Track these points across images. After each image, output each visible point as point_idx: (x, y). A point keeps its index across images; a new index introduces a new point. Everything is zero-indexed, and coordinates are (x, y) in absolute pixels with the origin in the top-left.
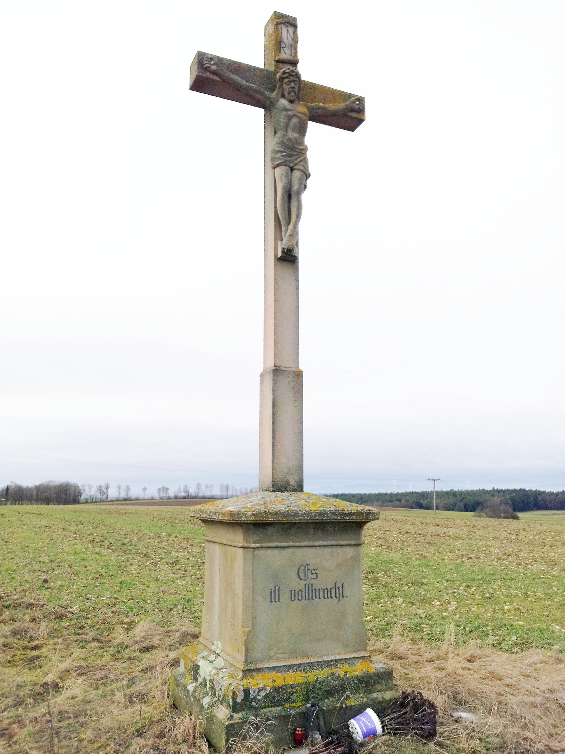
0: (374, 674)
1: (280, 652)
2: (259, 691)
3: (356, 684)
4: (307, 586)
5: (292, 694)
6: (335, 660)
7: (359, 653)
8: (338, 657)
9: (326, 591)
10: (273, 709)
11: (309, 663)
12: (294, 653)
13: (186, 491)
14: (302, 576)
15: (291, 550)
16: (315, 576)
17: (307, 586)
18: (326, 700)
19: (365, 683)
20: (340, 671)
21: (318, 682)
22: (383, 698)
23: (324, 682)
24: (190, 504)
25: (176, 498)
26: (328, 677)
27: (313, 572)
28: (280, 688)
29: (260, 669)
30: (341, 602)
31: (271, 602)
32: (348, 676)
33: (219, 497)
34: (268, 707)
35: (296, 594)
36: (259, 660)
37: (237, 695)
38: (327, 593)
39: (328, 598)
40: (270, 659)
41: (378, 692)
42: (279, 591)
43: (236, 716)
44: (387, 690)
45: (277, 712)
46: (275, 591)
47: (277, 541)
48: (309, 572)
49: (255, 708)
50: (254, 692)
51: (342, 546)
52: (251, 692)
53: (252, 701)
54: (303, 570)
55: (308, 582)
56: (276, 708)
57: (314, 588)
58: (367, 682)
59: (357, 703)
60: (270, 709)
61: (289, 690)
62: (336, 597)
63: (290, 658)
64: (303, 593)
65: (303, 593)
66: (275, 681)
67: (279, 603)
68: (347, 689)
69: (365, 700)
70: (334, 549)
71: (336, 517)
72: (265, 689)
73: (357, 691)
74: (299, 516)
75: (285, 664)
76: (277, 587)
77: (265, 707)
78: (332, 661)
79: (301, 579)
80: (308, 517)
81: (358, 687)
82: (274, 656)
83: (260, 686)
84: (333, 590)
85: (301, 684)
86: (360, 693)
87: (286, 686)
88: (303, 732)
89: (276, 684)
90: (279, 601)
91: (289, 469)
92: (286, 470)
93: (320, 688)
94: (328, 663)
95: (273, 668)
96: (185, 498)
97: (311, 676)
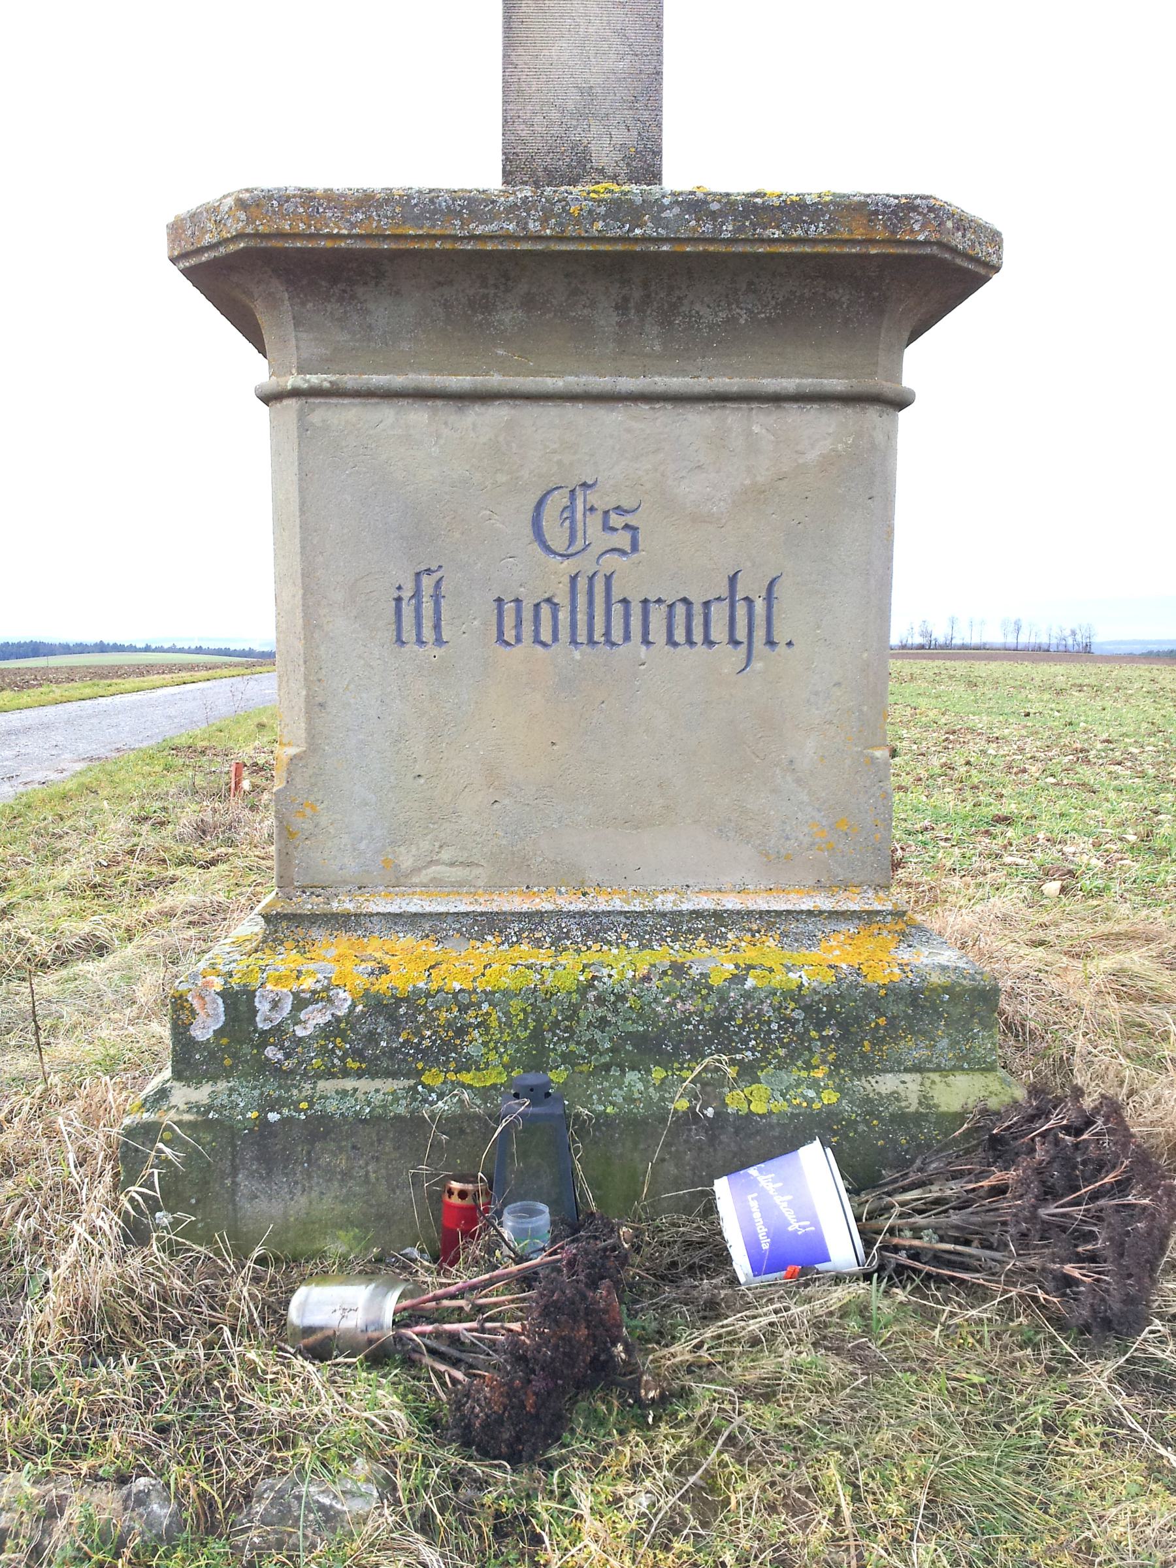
0: (892, 990)
1: (445, 855)
2: (300, 1003)
3: (793, 1023)
4: (582, 583)
5: (461, 1032)
6: (717, 915)
7: (842, 895)
8: (731, 903)
9: (680, 609)
10: (365, 1085)
11: (583, 914)
12: (514, 868)
13: (926, 634)
14: (556, 535)
15: (500, 413)
16: (622, 540)
17: (582, 583)
18: (632, 1076)
19: (843, 1026)
20: (715, 963)
21: (592, 995)
22: (924, 1099)
23: (621, 998)
24: (932, 657)
25: (904, 647)
26: (647, 978)
27: (616, 520)
28: (399, 1001)
29: (347, 916)
30: (757, 665)
31: (400, 641)
32: (750, 983)
33: (998, 646)
34: (346, 1073)
35: (528, 614)
36: (346, 883)
37: (193, 1013)
38: (687, 622)
39: (690, 642)
40: (398, 881)
41: (907, 1070)
42: (437, 598)
43: (182, 1095)
44: (954, 1069)
45: (377, 1099)
46: (417, 594)
47: (420, 368)
48: (595, 520)
49: (277, 1070)
50: (275, 1005)
51: (777, 399)
52: (263, 1006)
53: (264, 1045)
54: (557, 508)
55: (585, 564)
56: (378, 1083)
57: (616, 595)
58: (850, 1023)
59: (779, 1106)
60: (349, 1084)
61: (444, 1016)
62: (735, 643)
63: (493, 887)
64: (563, 615)
65: (563, 615)
66: (385, 970)
67: (438, 651)
68: (745, 1041)
69: (830, 1097)
70: (733, 417)
71: (707, 228)
72: (330, 1000)
73: (799, 1051)
74: (493, 217)
75: (463, 908)
76: (427, 582)
77: (330, 1075)
78: (697, 914)
79: (548, 550)
80: (544, 221)
81: (803, 1037)
82: (416, 870)
83: (308, 983)
84: (719, 613)
85: (506, 993)
86: (809, 1067)
87: (428, 995)
88: (468, 1201)
89: (383, 985)
90: (439, 641)
91: (587, 92)
92: (572, 100)
93: (603, 1022)
94: (680, 925)
95: (412, 920)
96: (922, 647)
97: (566, 969)
